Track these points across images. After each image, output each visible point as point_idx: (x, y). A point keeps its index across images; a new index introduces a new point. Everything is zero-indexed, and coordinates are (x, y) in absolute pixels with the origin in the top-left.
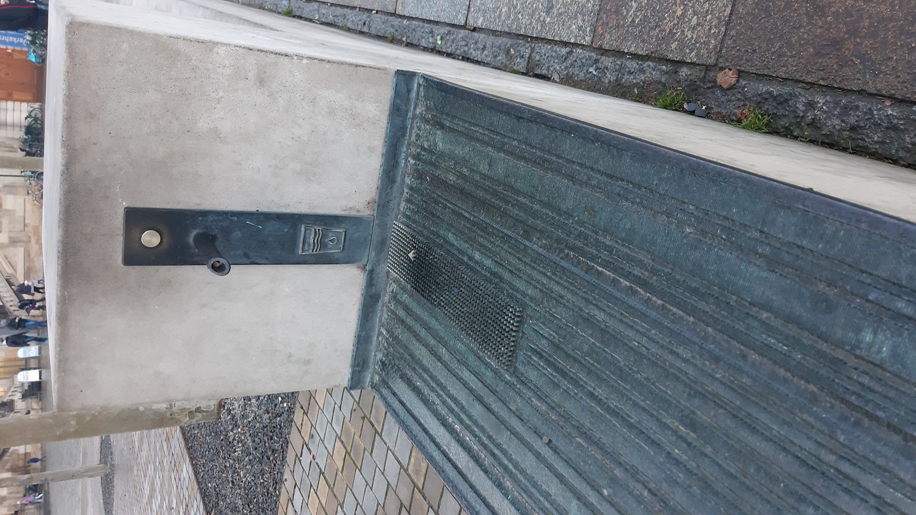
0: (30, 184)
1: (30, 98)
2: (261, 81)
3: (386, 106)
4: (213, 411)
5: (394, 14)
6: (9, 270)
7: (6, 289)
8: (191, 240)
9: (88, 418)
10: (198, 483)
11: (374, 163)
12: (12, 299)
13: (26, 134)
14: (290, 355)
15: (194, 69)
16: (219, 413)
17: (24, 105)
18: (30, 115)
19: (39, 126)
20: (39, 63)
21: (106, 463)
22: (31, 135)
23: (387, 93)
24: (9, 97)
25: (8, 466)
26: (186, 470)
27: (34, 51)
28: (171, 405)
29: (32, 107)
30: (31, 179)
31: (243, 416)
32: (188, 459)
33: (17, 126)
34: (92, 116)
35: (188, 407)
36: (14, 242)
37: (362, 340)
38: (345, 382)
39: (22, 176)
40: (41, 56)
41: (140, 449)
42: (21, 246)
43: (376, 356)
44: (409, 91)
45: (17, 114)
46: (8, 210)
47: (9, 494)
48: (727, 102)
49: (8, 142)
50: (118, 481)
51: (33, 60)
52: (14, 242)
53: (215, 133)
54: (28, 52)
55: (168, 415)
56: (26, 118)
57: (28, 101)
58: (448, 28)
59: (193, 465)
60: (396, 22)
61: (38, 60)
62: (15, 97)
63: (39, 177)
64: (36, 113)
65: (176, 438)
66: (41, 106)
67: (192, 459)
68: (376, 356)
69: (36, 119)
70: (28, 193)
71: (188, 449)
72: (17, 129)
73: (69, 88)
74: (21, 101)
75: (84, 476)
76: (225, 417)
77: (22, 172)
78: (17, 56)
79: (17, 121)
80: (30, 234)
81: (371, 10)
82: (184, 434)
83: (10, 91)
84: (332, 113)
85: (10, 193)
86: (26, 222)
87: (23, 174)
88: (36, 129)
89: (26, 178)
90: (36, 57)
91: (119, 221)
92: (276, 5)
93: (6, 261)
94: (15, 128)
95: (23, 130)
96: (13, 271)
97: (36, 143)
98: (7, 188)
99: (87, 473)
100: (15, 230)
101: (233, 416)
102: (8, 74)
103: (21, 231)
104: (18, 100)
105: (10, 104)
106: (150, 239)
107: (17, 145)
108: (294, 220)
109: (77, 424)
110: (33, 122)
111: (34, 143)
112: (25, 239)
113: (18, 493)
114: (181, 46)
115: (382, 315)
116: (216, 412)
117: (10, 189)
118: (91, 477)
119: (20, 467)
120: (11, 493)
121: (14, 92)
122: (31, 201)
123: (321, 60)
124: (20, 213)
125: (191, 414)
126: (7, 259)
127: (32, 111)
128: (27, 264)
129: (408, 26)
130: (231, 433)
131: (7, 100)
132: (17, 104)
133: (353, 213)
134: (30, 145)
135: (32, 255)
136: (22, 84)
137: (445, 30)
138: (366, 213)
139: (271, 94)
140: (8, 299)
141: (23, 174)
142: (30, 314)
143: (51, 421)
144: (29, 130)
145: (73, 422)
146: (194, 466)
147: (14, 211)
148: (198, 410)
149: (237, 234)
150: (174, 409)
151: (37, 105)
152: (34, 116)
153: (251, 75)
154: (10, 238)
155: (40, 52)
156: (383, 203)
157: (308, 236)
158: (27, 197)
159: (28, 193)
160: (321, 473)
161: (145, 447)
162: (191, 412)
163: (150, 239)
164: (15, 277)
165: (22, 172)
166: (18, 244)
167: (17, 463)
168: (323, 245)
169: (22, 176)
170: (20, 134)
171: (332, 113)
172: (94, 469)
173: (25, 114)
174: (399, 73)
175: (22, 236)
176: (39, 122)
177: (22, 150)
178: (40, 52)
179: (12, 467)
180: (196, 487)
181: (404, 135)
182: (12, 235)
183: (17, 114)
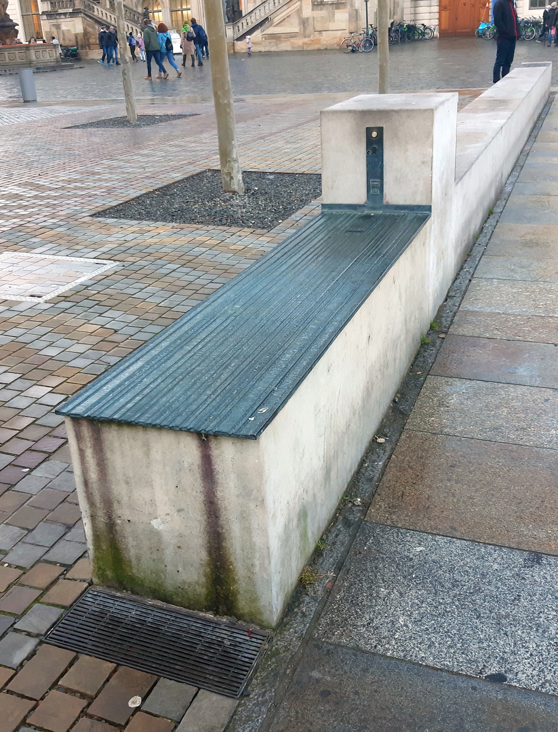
0: (360, 34)
1: (443, 27)
2: (423, 163)
3: (420, 204)
4: (231, 187)
5: (483, 255)
6: (276, 20)
7: (258, 18)
8: (374, 146)
9: (228, 110)
10: (173, 183)
11: (401, 202)
12: (249, 24)
13: (408, 26)
14: (335, 181)
15: (425, 143)
16: (229, 192)
17: (436, 22)
18: (427, 28)
19: (416, 37)
20: (478, 32)
21: (138, 120)
22: (407, 31)
23: (424, 203)
24: (442, 8)
25: (90, 29)
26: (178, 176)
27: (489, 28)
28: (235, 161)
29: (434, 29)
30: (365, 35)
31: (232, 206)
32: (186, 176)
33: (415, 17)
34: (409, 116)
35: (234, 172)
36: (304, 22)
37: (340, 206)
38: (324, 203)
39: (367, 26)
40: (484, 35)
41: (171, 146)
42: (300, 30)
43: (334, 211)
44: (425, 210)
45: (427, 16)
46: (334, 14)
47: (63, 31)
48: (484, 666)
49: (399, 11)
50: (125, 131)
51: (480, 28)
52: (304, 22)
53: (407, 150)
54: (488, 22)
55: (228, 159)
56: (423, 25)
57: (440, 25)
58: (472, 273)
59: (183, 180)
60: (479, 256)
61: (480, 32)
62: (443, 13)
63: (368, 41)
64: (429, 34)
65: (195, 168)
66: (436, 37)
67: (187, 179)
68: (334, 211)
69: (423, 34)
70: (351, 33)
71: (192, 176)
72: (412, 17)
73: (416, 110)
74: (440, 19)
75: (127, 104)
76: (227, 195)
77: (371, 25)
78: (483, 12)
79: (419, 16)
80: (312, 37)
81: (486, 246)
82: (200, 173)
83: (448, 8)
84: (416, 186)
85: (350, 15)
86: (324, 33)
87: (369, 26)
88: (413, 35)
89: (365, 30)
90: (483, 29)
91: (379, 125)
92: (498, 207)
93: (286, 17)
94: (413, 9)
95: (412, 23)
96: (275, 24)
97: (400, 36)
98: (355, 13)
99: (130, 106)
100: (315, 22)
101: (229, 200)
102: (465, 5)
103: (314, 28)
104: (440, 16)
105: (436, 9)
106: (374, 134)
107: (397, 18)
108: (381, 177)
109: (225, 104)
110: (420, 32)
111: (399, 34)
112: (307, 32)
113: (64, 39)
114: (430, 139)
115: (349, 212)
116: (230, 190)
117: (355, 16)
118: (127, 109)
119: (88, 40)
120: (63, 33)
121: (448, 11)
122: (344, 35)
123: (432, 180)
124: (332, 26)
125: (229, 174)
126: (288, 17)
127: (430, 29)
128: (283, 36)
129: (475, 260)
130: (219, 199)
131: (440, 6)
132: (437, 15)
133: (384, 197)
134: (398, 30)
135: (292, 40)
136: (457, 19)
137: (472, 272)
138: (385, 202)
139: (419, 166)
140: (249, 21)
141: (369, 26)
142: (235, 41)
143: (227, 88)
144: (412, 28)
145: (226, 102)
146: (182, 181)
147: (334, 21)
148: (232, 178)
149: (376, 160)
150: (233, 163)
151: (436, 33)
152: (426, 31)
153: (425, 160)
154: (308, 19)
155: (488, 33)
156: (389, 207)
157: (377, 183)
158: (347, 31)
159: (351, 33)
160: (223, 241)
161: (174, 149)
162: (230, 174)
163: (374, 134)
164: (271, 26)
165: (371, 25)
166: (302, 26)
167: (93, 37)
168: (373, 187)
169: (367, 26)
170: (408, 20)
171: (416, 186)
172: (133, 112)
173: (427, 23)
174: (431, 206)
175: (310, 29)
176: (421, 37)
177: (392, 24)
178: (488, 33)
179: (89, 33)
180: (171, 182)
181: (411, 211)
182: (311, 21)
183: (427, 16)
